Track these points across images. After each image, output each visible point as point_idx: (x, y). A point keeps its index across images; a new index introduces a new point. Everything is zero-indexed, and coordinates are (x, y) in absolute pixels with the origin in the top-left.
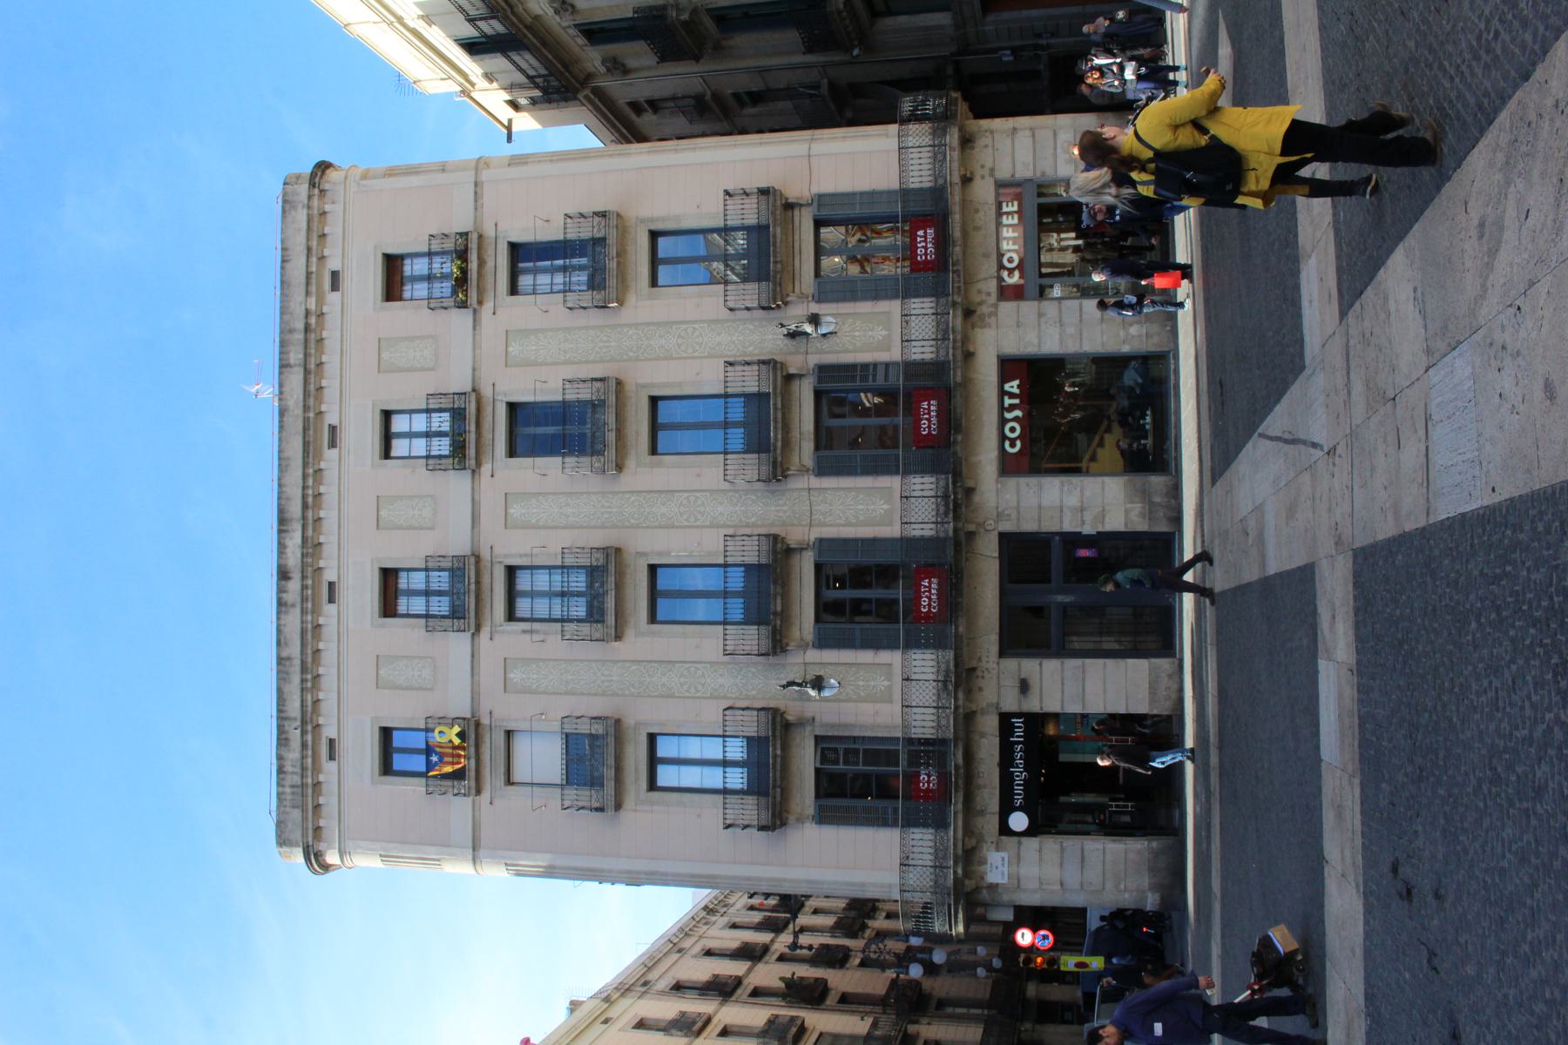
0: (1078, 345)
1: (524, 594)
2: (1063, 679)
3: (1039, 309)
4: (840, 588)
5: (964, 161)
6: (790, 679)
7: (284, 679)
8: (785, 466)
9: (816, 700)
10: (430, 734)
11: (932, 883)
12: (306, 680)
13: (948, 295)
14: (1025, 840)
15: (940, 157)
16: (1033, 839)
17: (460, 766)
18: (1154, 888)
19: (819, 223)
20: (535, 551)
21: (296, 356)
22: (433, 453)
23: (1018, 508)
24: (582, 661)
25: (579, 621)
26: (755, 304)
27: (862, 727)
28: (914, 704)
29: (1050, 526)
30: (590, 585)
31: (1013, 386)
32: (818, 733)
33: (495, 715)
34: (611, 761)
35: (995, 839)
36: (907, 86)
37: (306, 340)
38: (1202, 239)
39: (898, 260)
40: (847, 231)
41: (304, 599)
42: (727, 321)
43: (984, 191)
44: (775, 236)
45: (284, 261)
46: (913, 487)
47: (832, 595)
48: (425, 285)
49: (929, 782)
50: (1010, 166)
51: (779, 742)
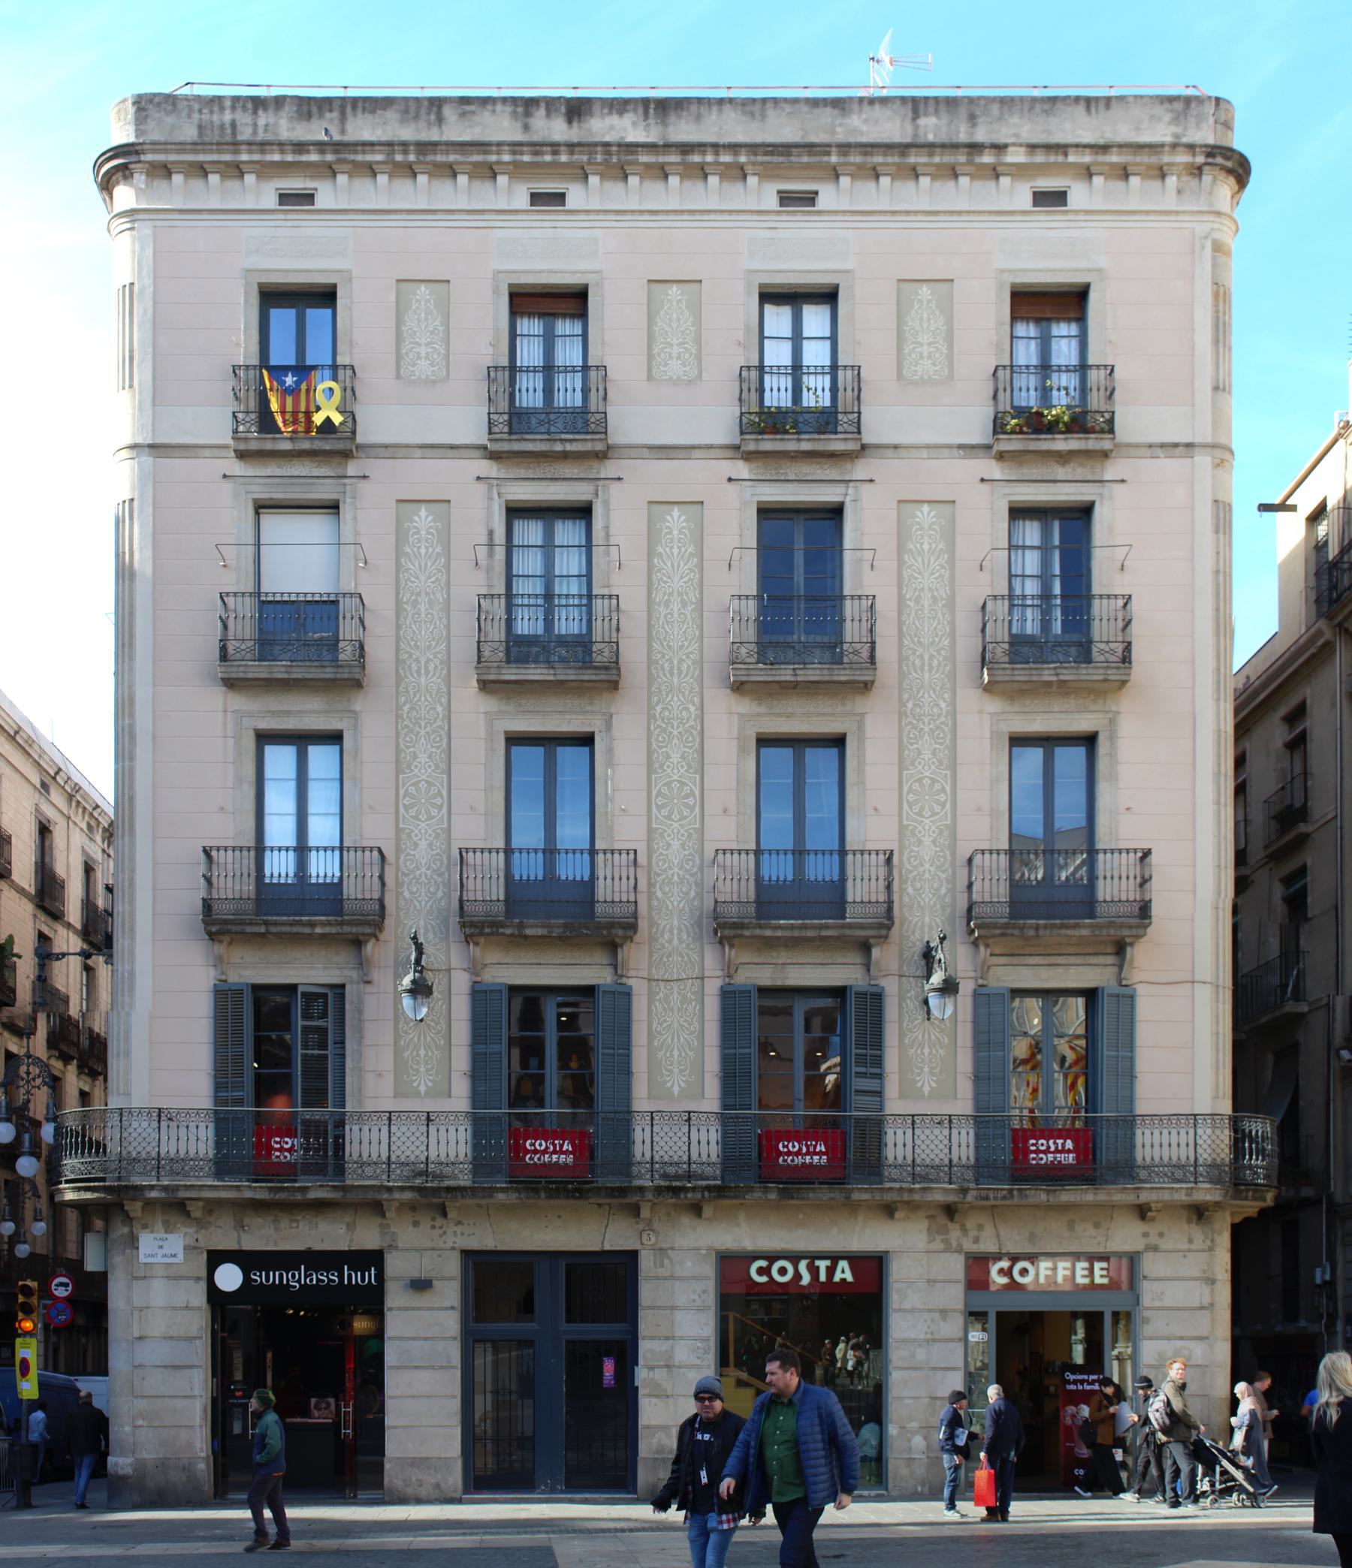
0: (900, 1364)
1: (549, 534)
2: (432, 1339)
3: (954, 1311)
4: (559, 1022)
5: (1170, 1208)
6: (427, 948)
7: (406, 112)
8: (736, 941)
9: (396, 988)
10: (327, 373)
11: (134, 1154)
12: (405, 152)
13: (977, 1181)
14: (203, 1286)
15: (1179, 1174)
16: (205, 1298)
17: (281, 425)
18: (140, 1467)
19: (1091, 995)
20: (614, 550)
21: (932, 128)
22: (767, 378)
23: (672, 1277)
24: (448, 627)
25: (510, 622)
26: (975, 897)
27: (359, 1054)
28: (393, 1128)
29: (646, 1322)
30: (563, 641)
31: (844, 1272)
32: (348, 987)
33: (362, 485)
34: (298, 673)
35: (202, 1244)
36: (1289, 1130)
37: (955, 146)
38: (1042, 1535)
39: (1032, 1111)
40: (1078, 1037)
41: (536, 147)
42: (954, 855)
43: (1126, 1236)
44: (1076, 926)
45: (1088, 102)
46: (703, 1130)
47: (550, 1011)
48: (1034, 361)
49: (281, 1150)
50: (1161, 1275)
51: (334, 930)
